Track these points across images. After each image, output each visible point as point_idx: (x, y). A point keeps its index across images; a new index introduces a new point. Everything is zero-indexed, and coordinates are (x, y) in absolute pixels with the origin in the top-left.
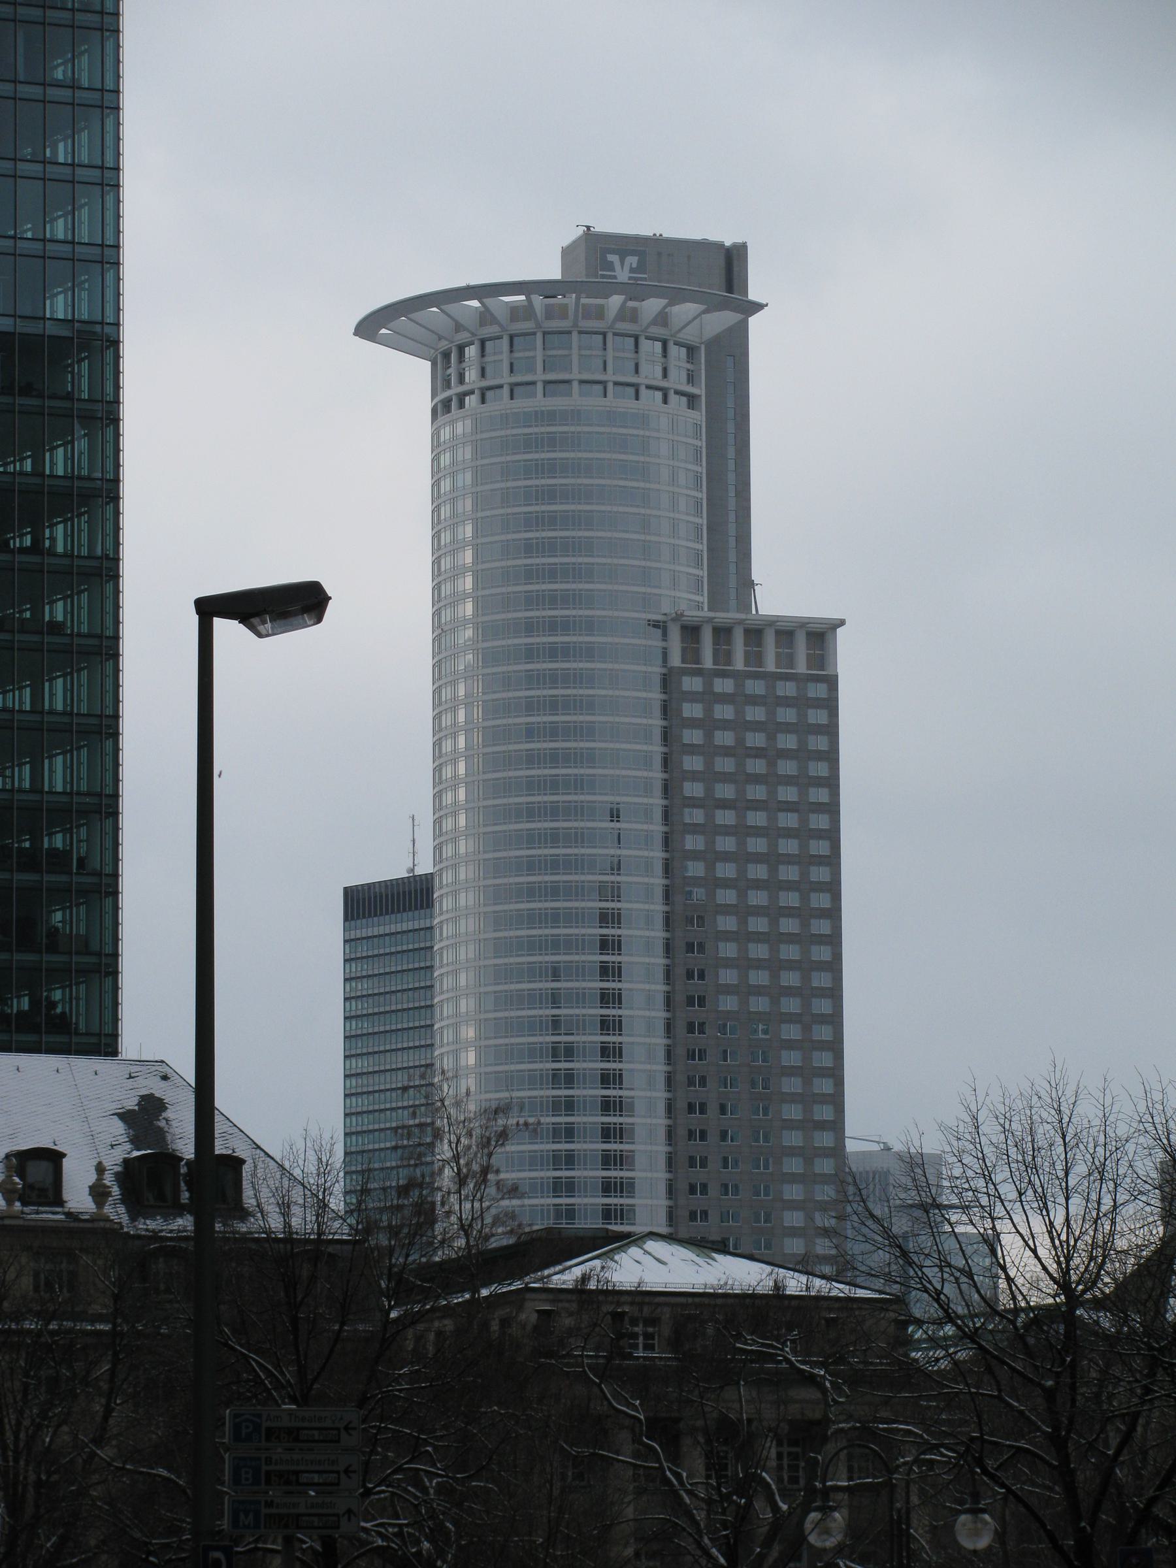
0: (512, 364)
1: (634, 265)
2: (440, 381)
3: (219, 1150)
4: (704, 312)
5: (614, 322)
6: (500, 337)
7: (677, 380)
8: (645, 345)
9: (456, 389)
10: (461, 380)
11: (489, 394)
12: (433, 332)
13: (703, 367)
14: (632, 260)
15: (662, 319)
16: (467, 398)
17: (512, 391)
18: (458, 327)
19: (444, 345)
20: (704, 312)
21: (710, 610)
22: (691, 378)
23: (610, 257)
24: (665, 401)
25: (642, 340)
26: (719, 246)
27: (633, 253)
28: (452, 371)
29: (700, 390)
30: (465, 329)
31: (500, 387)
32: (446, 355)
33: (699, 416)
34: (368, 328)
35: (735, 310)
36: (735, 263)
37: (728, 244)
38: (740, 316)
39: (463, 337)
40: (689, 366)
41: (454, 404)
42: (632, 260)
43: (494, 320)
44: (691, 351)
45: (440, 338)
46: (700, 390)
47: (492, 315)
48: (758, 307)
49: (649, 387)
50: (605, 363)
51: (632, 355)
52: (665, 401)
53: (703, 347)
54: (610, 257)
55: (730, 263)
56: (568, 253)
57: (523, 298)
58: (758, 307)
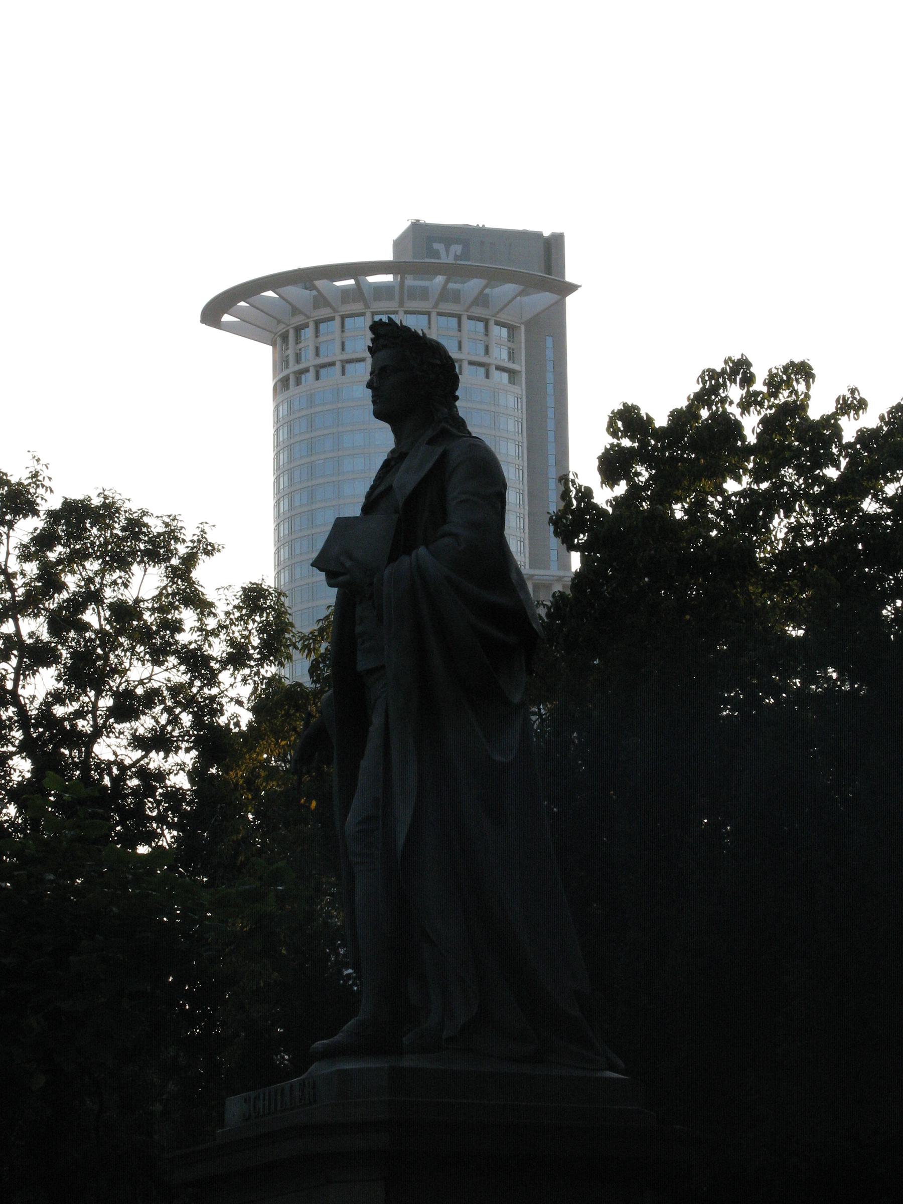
0: (343, 344)
1: (458, 253)
2: (281, 362)
3: (661, 421)
4: (486, 287)
5: (470, 307)
6: (332, 319)
7: (500, 355)
8: (467, 324)
9: (293, 367)
10: (298, 359)
11: (323, 372)
12: (271, 316)
13: (523, 345)
14: (457, 249)
15: (482, 300)
16: (303, 376)
17: (343, 368)
18: (295, 311)
19: (281, 328)
20: (520, 294)
21: (530, 568)
22: (512, 356)
23: (436, 246)
24: (487, 376)
25: (465, 322)
26: (538, 235)
27: (456, 241)
28: (291, 352)
29: (520, 366)
30: (301, 313)
31: (332, 364)
32: (285, 337)
33: (520, 389)
34: (212, 314)
35: (551, 290)
36: (553, 251)
37: (546, 234)
38: (559, 297)
39: (299, 320)
40: (509, 344)
41: (292, 381)
42: (457, 249)
43: (327, 304)
44: (512, 329)
45: (279, 322)
46: (520, 366)
47: (324, 298)
48: (572, 288)
49: (471, 363)
50: (460, 343)
51: (456, 333)
52: (487, 376)
53: (523, 328)
54: (436, 246)
55: (550, 249)
56: (398, 244)
57: (351, 282)
58: (572, 288)
